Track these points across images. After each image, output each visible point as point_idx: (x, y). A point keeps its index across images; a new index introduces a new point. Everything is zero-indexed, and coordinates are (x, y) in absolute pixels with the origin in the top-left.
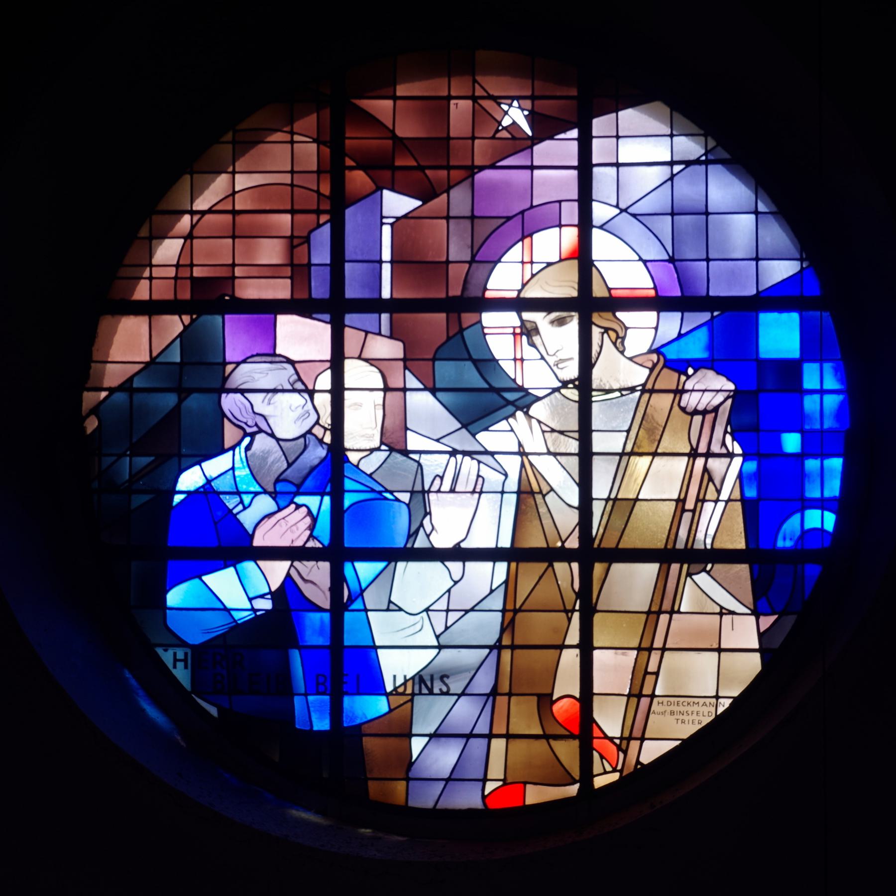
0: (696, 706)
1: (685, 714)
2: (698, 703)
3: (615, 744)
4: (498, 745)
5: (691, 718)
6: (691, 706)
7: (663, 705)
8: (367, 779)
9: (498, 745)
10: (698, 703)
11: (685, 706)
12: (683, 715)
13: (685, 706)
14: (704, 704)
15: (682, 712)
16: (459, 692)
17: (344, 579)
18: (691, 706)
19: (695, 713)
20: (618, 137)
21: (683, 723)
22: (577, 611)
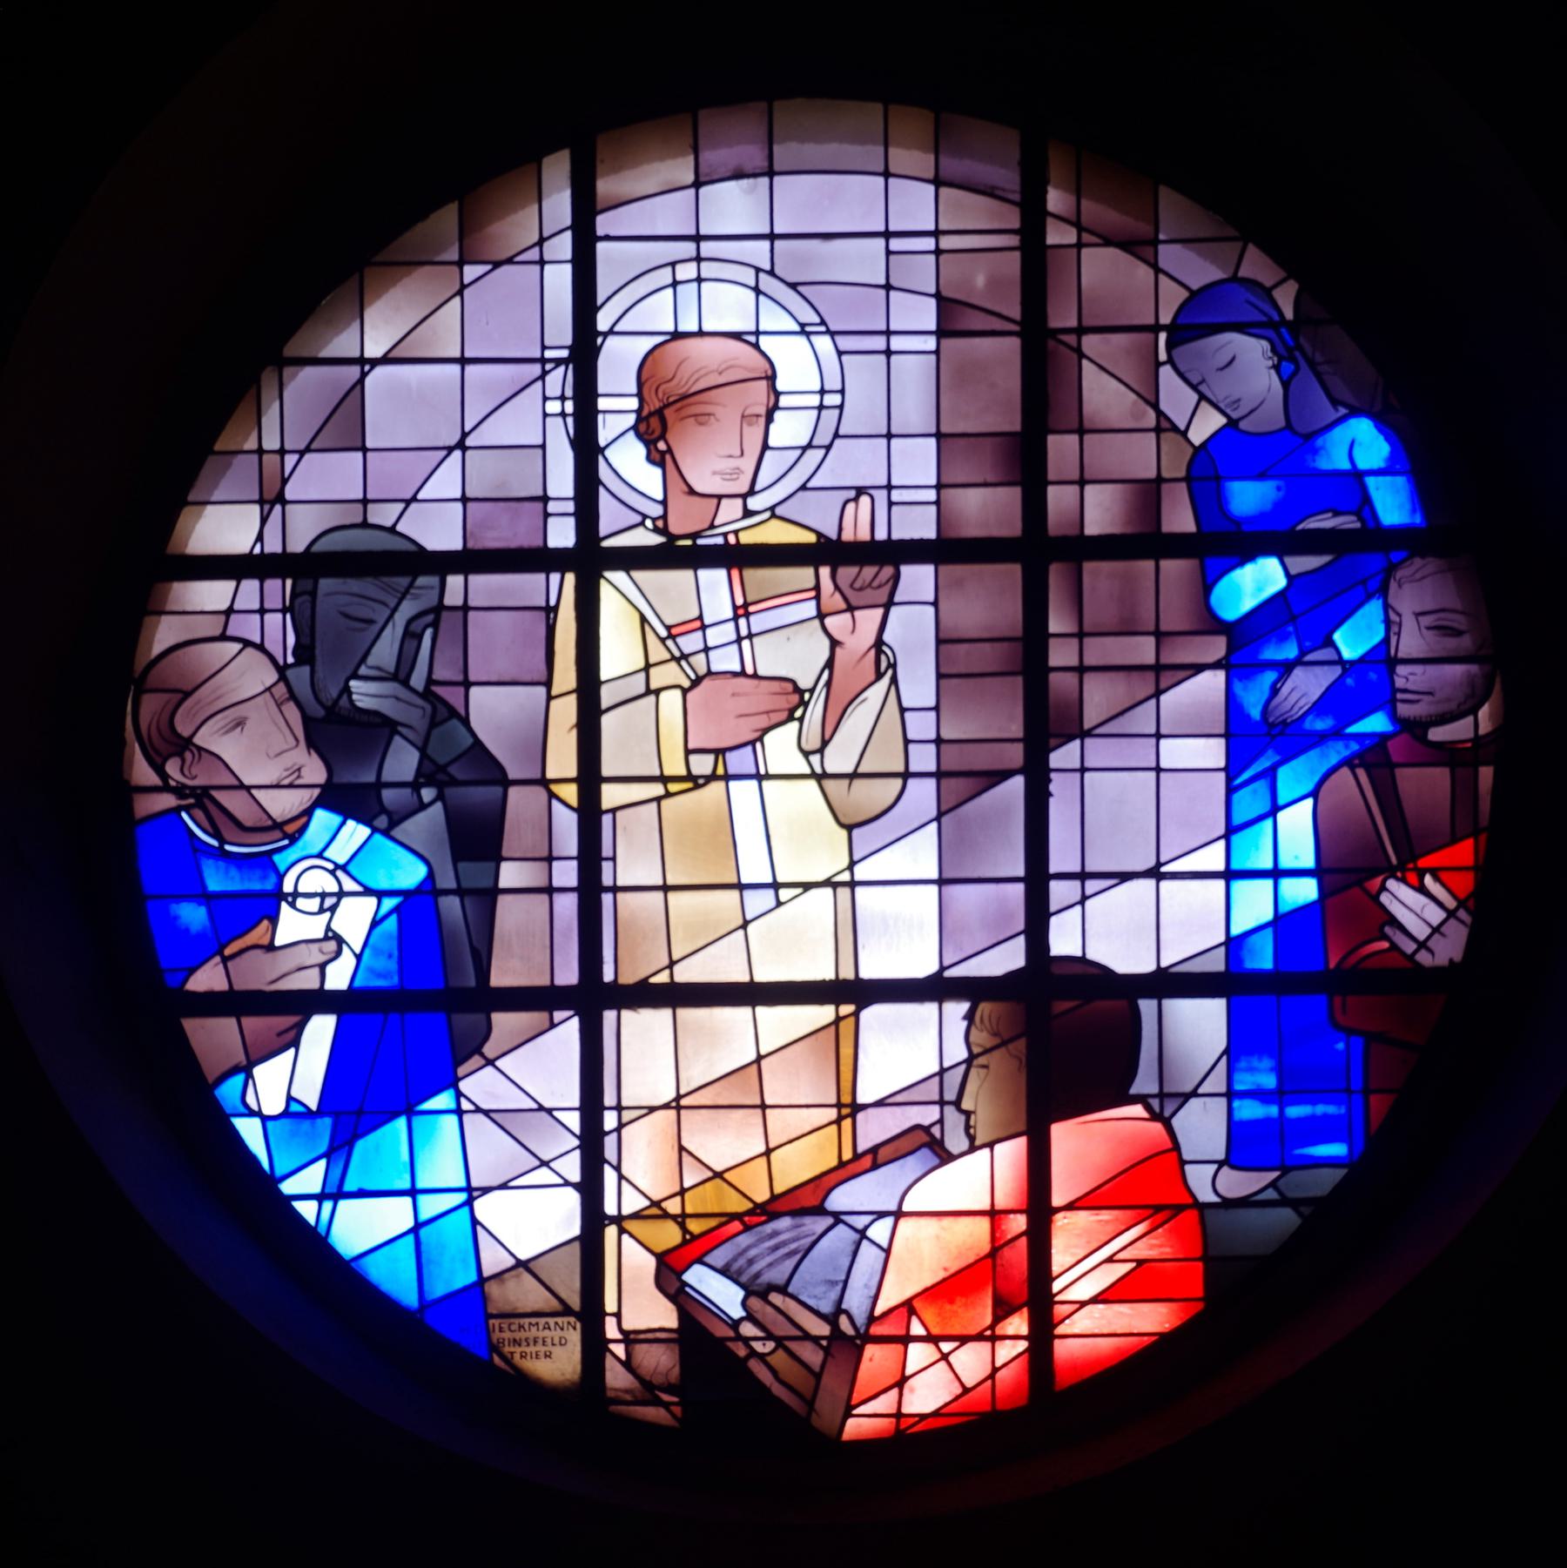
0: (534, 1329)
1: (524, 1343)
2: (537, 1324)
3: (821, 1347)
4: (754, 869)
5: (532, 1349)
6: (525, 1330)
7: (974, 1112)
8: (1476, 868)
9: (272, 442)
10: (537, 1324)
11: (515, 1331)
12: (562, 1329)
13: (515, 1331)
14: (547, 1326)
15: (570, 1327)
16: (302, 446)
17: (169, 776)
18: (525, 1330)
19: (541, 1341)
20: (889, 436)
21: (548, 1359)
22: (1164, 363)
